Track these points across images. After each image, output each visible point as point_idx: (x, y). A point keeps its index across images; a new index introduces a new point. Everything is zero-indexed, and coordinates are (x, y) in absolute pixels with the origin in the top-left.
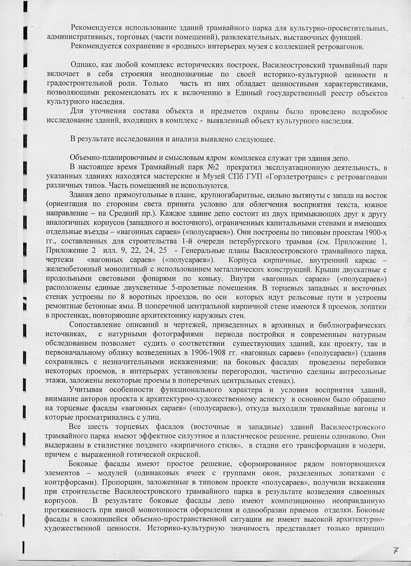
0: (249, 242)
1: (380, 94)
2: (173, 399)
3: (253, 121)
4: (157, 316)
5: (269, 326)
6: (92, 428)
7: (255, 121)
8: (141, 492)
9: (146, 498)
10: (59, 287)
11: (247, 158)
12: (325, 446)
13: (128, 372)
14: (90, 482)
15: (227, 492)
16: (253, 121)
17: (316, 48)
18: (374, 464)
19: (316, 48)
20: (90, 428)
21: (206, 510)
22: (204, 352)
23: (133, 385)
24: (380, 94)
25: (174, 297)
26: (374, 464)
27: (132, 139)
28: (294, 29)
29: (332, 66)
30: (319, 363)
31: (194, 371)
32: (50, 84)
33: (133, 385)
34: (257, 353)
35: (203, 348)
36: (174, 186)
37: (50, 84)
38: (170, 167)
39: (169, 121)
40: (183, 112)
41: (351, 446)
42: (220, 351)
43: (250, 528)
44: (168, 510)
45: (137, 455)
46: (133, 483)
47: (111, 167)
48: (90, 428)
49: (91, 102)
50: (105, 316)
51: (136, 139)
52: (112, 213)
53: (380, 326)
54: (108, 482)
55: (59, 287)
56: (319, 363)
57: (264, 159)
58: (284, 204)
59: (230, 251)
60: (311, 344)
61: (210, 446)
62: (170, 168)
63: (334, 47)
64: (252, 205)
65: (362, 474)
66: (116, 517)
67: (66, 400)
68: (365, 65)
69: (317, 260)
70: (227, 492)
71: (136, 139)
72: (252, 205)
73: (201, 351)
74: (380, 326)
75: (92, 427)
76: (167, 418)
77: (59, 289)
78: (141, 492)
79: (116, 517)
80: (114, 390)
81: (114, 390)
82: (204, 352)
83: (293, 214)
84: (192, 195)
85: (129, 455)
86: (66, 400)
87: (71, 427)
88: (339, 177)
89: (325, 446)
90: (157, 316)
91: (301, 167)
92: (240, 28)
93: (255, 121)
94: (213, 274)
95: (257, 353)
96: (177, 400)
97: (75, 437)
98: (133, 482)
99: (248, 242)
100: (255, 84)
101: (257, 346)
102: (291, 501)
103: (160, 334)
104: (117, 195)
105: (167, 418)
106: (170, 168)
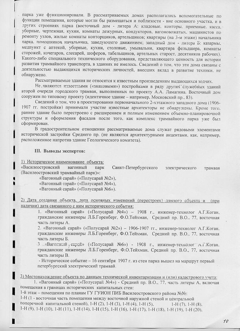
0: (139, 168)
5: (92, 15)
8: (38, 168)
10: (80, 64)
12: (60, 119)
14: (218, 130)
15: (156, 168)
18: (73, 70)
20: (88, 54)
21: (60, 118)
26: (73, 70)
27: (183, 168)
28: (69, 31)
30: (46, 173)
31: (89, 21)
32: (39, 217)
37: (39, 217)
43: (63, 162)
45: (86, 129)
47: (62, 218)
48: (88, 54)
50: (24, 91)
51: (27, 47)
55: (80, 64)
56: (46, 173)
60: (83, 53)
66: (81, 52)
67: (52, 234)
68: (82, 173)
70: (90, 135)
71: (27, 47)
77: (80, 65)
78: (38, 168)
79: (81, 52)
83: (65, 113)
84: (67, 113)
85: (57, 92)
86: (52, 234)
87: (190, 93)
89: (60, 119)
92: (179, 119)
96: (34, 118)
97: (58, 65)
99: (138, 168)
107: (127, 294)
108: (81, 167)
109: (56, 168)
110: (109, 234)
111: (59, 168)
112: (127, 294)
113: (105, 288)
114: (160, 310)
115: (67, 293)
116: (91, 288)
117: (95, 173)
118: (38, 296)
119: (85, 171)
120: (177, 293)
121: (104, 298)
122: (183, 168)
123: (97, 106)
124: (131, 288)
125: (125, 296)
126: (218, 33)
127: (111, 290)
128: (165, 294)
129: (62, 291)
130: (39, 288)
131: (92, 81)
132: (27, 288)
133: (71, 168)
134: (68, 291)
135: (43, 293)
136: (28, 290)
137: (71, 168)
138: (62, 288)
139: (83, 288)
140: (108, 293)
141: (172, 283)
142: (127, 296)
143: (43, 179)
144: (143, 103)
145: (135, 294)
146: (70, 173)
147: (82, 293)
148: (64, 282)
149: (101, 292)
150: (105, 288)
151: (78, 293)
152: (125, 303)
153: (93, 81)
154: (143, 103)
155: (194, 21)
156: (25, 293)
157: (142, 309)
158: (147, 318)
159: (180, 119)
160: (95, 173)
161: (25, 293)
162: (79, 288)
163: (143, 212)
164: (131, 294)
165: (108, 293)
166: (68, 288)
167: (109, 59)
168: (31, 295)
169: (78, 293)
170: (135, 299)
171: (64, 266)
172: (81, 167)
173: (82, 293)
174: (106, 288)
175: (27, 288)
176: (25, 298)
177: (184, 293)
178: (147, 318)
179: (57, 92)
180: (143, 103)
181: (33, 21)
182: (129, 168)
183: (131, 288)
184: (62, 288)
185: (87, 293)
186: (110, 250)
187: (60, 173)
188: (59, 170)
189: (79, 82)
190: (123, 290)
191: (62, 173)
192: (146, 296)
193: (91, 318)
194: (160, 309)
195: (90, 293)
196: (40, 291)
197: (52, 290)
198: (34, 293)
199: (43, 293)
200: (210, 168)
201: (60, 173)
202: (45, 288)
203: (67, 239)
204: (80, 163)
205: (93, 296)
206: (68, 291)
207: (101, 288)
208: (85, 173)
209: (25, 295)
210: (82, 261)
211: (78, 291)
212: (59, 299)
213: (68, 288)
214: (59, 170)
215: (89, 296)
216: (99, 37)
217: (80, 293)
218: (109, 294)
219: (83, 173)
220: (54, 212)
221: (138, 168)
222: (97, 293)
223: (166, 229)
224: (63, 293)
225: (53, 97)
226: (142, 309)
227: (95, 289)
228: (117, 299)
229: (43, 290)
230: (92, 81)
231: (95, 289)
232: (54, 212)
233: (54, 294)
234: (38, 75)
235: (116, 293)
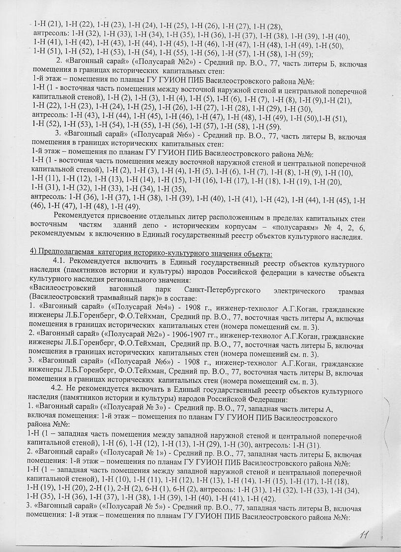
0: (229, 290)
1: (116, 399)
2: (289, 291)
11: (161, 516)
13: (147, 271)
15: (259, 291)
17: (230, 236)
19: (230, 236)
22: (184, 335)
23: (130, 276)
24: (116, 399)
27: (304, 292)
28: (327, 265)
33: (130, 276)
34: (83, 61)
35: (184, 330)
38: (124, 298)
40: (306, 265)
41: (298, 273)
42: (194, 361)
49: (73, 279)
53: (358, 365)
54: (44, 251)
57: (333, 237)
58: (357, 237)
59: (159, 515)
61: (152, 280)
65: (311, 274)
68: (255, 263)
70: (259, 291)
73: (194, 363)
74: (358, 365)
76: (75, 425)
82: (184, 335)
88: (266, 264)
91: (275, 400)
95: (83, 61)
97: (270, 346)
99: (227, 290)
101: (328, 276)
105: (75, 425)
107: (213, 81)
109: (89, 289)
110: (102, 343)
111: (94, 288)
112: (213, 81)
113: (176, 71)
114: (272, 182)
115: (113, 80)
116: (153, 71)
117: (156, 299)
118: (64, 83)
119: (139, 294)
120: (297, 81)
121: (171, 471)
124: (219, 145)
125: (210, 85)
127: (186, 148)
128: (277, 155)
129: (103, 148)
130: (64, 143)
132: (44, 70)
133: (115, 289)
134: (114, 148)
135: (70, 152)
136: (44, 147)
137: (115, 289)
138: (104, 143)
139: (138, 144)
140: (180, 152)
141: (290, 64)
142: (213, 85)
143: (71, 134)
145: (226, 154)
146: (112, 297)
147: (138, 80)
148: (107, 134)
149: (169, 78)
150: (176, 71)
151: (130, 153)
152: (263, 479)
153: (151, 217)
156: (40, 151)
157: (241, 180)
160: (156, 299)
161: (41, 78)
162: (133, 71)
164: (219, 154)
165: (180, 152)
166: (113, 143)
167: (259, 236)
168: (52, 82)
169: (130, 153)
170: (227, 90)
173: (138, 80)
174: (179, 71)
175: (44, 70)
176: (41, 160)
177: (309, 82)
182: (213, 290)
183: (219, 145)
184: (104, 143)
185: (146, 80)
186: (102, 343)
187: (96, 298)
188: (95, 293)
190: (207, 75)
191: (100, 298)
192: (245, 86)
194: (272, 181)
195: (150, 152)
196: (66, 148)
197: (86, 148)
198: (55, 152)
199: (70, 152)
200: (348, 292)
201: (96, 298)
202: (75, 70)
205: (156, 157)
206: (115, 75)
207: (39, 170)
208: (139, 298)
209: (42, 82)
210: (83, 398)
211: (132, 76)
212: (97, 161)
213: (113, 143)
214: (95, 293)
215: (150, 84)
216: (118, 399)
217: (134, 80)
218: (183, 81)
219: (135, 298)
221: (227, 290)
222: (163, 80)
224: (106, 80)
226: (241, 180)
227: (160, 74)
228: (77, 89)
229: (71, 147)
231: (160, 74)
233: (90, 80)
234: (229, 363)
235: (194, 153)
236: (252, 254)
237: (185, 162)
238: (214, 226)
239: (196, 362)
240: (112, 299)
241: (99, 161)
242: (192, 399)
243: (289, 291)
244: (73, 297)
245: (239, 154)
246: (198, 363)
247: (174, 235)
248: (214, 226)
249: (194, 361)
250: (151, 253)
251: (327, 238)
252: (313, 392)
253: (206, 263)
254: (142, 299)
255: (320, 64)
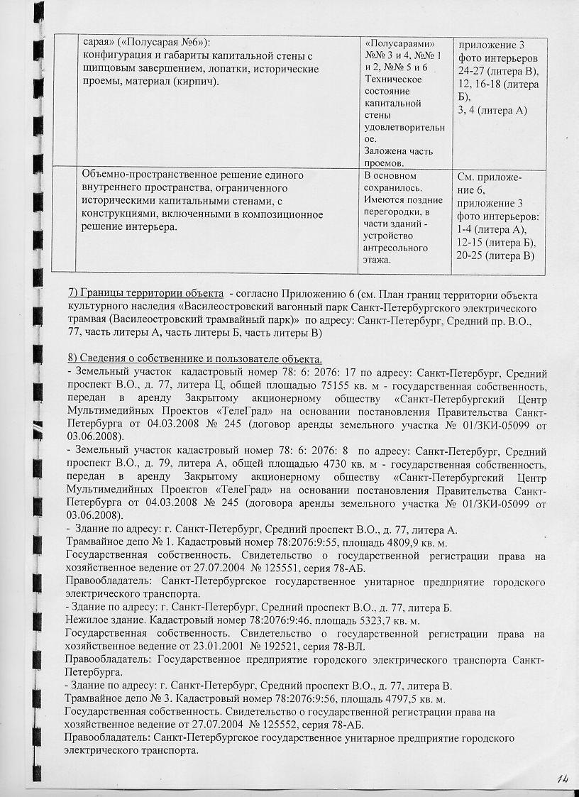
2: (85, 751)
3: (503, 296)
4: (501, 243)
6: (170, 70)
7: (506, 296)
9: (155, 577)
16: (503, 296)
20: (86, 69)
25: (95, 81)
27: (416, 661)
28: (73, 306)
29: (148, 594)
30: (217, 451)
34: (294, 308)
36: (112, 607)
38: (107, 541)
39: (255, 582)
42: (191, 422)
44: (130, 712)
46: (268, 479)
52: (158, 737)
53: (74, 751)
56: (217, 451)
62: (107, 543)
63: (528, 217)
64: (233, 386)
69: (232, 476)
71: (117, 410)
72: (233, 386)
74: (74, 751)
75: (198, 83)
80: (305, 412)
81: (305, 412)
90: (501, 243)
92: (275, 189)
93: (506, 296)
94: (142, 601)
95: (294, 308)
98: (268, 477)
99: (234, 608)
100: (93, 633)
102: (270, 215)
103: (467, 217)
104: (249, 659)
106: (107, 543)
108: (141, 410)
117: (291, 321)
122: (416, 661)
123: (314, 734)
126: (529, 71)
131: (177, 725)
144: (382, 504)
153: (181, 725)
154: (382, 504)
155: (512, 738)
158: (372, 765)
159: (385, 504)
160: (291, 321)
163: (109, 438)
171: (482, 321)
172: (141, 410)
178: (372, 765)
179: (394, 465)
180: (382, 504)
181: (265, 478)
187: (205, 320)
189: (415, 481)
193: (174, 771)
201: (205, 320)
203: (236, 334)
204: (115, 360)
207: (169, 202)
216: (100, 201)
220: (290, 307)
221: (234, 608)
223: (317, 295)
225: (264, 214)
230: (177, 725)
232: (290, 307)
236: (198, 294)
237: (92, 660)
238: (105, 410)
239: (194, 423)
240: (91, 543)
241: (145, 450)
242: (332, 660)
243: (85, 751)
244: (528, 217)
245: (460, 557)
246: (196, 425)
247: (265, 738)
248: (105, 410)
249: (191, 422)
250: (145, 293)
251: (137, 595)
252: (271, 426)
253: (400, 387)
254: (329, 309)
255: (138, 333)
